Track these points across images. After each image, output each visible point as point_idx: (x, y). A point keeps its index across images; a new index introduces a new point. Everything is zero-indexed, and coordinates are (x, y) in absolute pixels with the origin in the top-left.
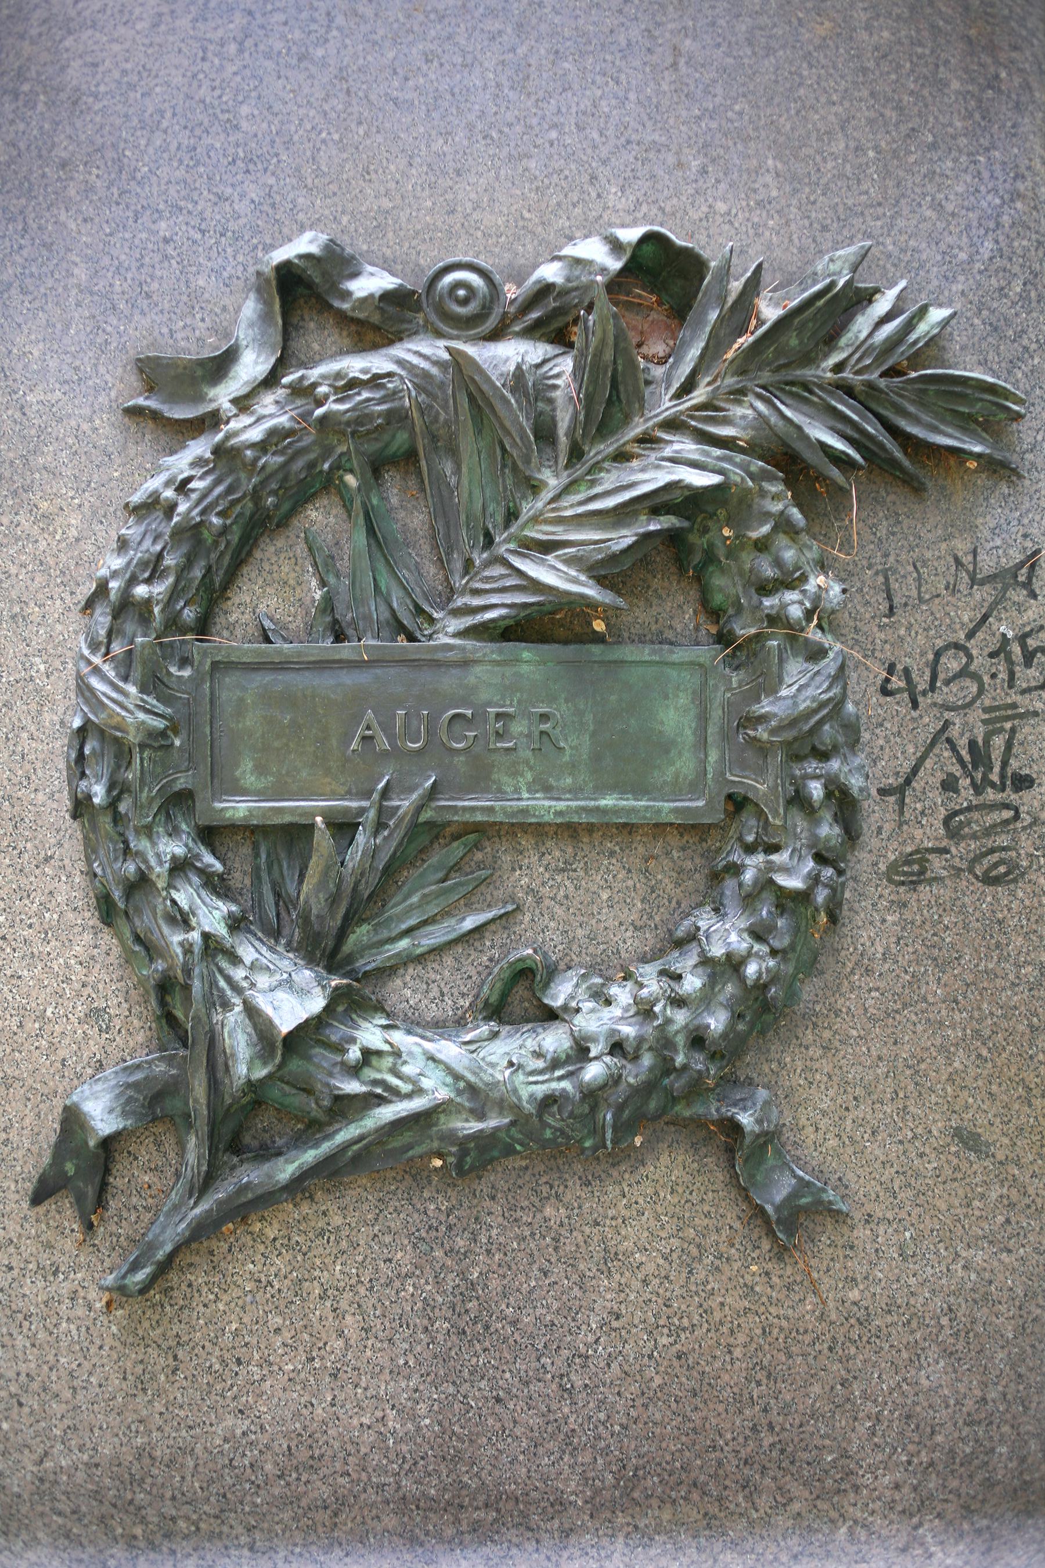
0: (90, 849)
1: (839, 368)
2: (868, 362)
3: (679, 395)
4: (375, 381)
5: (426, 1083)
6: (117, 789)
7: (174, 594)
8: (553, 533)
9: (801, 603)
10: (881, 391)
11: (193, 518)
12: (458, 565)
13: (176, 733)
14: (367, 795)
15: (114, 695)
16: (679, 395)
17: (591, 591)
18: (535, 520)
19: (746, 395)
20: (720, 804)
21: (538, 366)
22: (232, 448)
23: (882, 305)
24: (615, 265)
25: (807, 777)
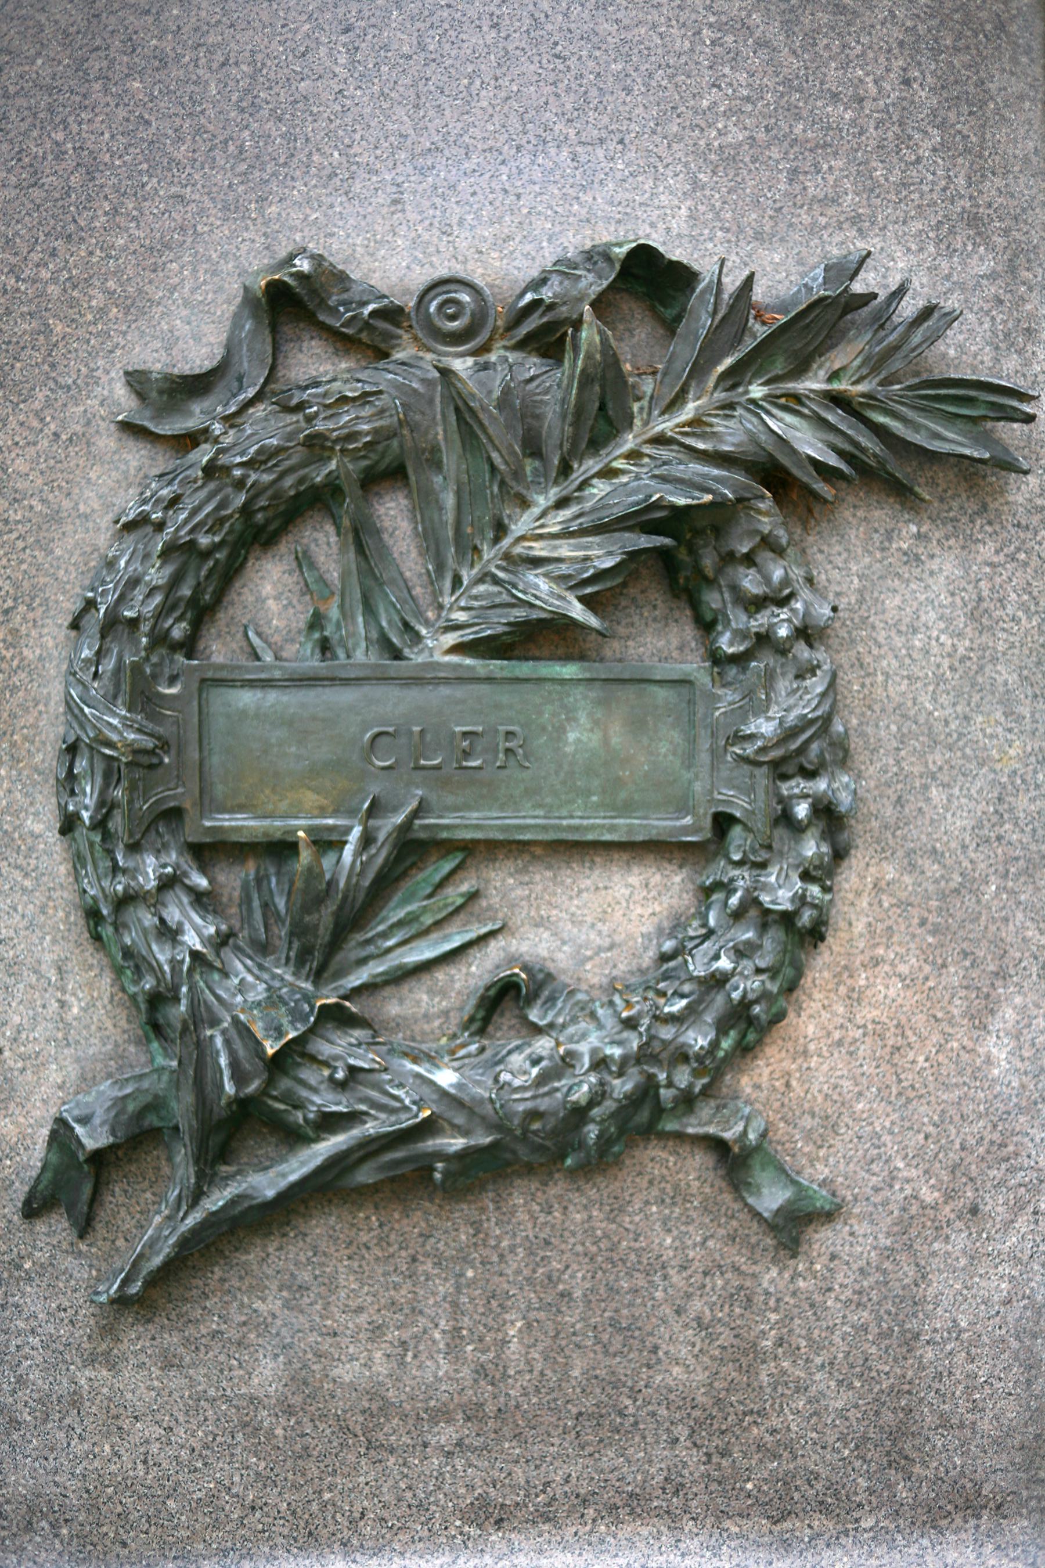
0: (78, 860)
6: (106, 807)
7: (161, 613)
9: (789, 621)
11: (181, 537)
12: (448, 584)
13: (167, 752)
14: (352, 813)
17: (577, 611)
19: (734, 409)
20: (708, 823)
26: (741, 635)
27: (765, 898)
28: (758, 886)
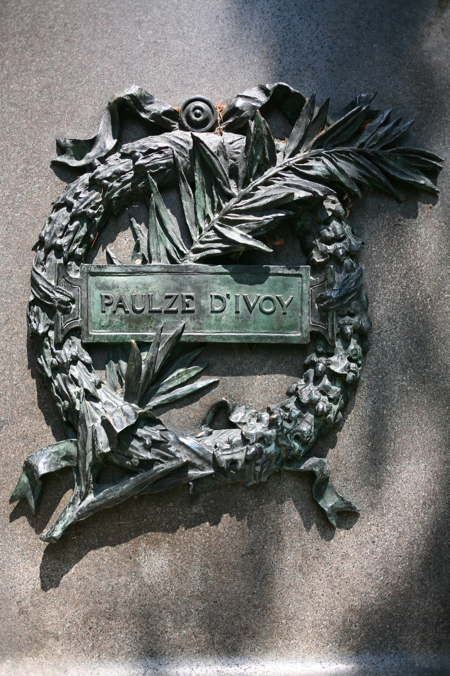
1: (362, 145)
2: (375, 143)
3: (292, 155)
4: (160, 150)
5: (178, 455)
8: (236, 217)
10: (380, 156)
15: (46, 286)
16: (292, 155)
18: (230, 212)
21: (231, 143)
22: (98, 179)
23: (380, 120)
24: (263, 99)
25: (345, 324)
26: (323, 254)
27: (332, 367)
28: (327, 364)
